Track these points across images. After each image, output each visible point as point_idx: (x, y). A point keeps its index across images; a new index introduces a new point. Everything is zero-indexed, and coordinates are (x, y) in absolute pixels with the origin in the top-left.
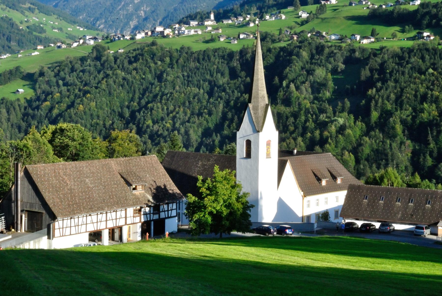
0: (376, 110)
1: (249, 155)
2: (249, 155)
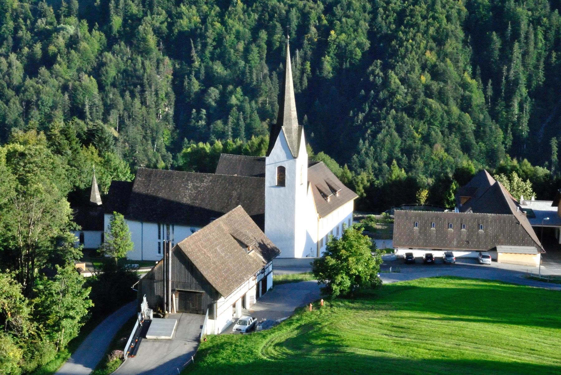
0: (117, 13)
1: (282, 183)
2: (282, 183)
